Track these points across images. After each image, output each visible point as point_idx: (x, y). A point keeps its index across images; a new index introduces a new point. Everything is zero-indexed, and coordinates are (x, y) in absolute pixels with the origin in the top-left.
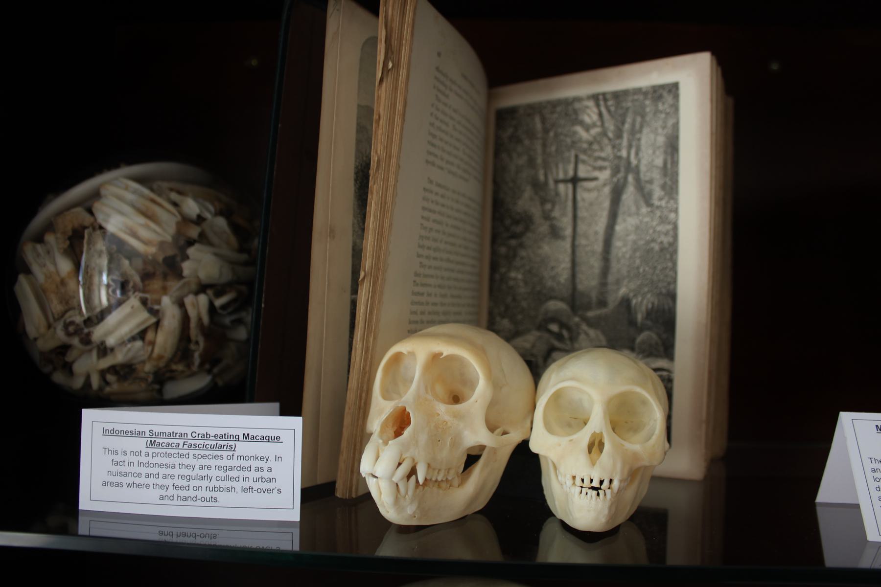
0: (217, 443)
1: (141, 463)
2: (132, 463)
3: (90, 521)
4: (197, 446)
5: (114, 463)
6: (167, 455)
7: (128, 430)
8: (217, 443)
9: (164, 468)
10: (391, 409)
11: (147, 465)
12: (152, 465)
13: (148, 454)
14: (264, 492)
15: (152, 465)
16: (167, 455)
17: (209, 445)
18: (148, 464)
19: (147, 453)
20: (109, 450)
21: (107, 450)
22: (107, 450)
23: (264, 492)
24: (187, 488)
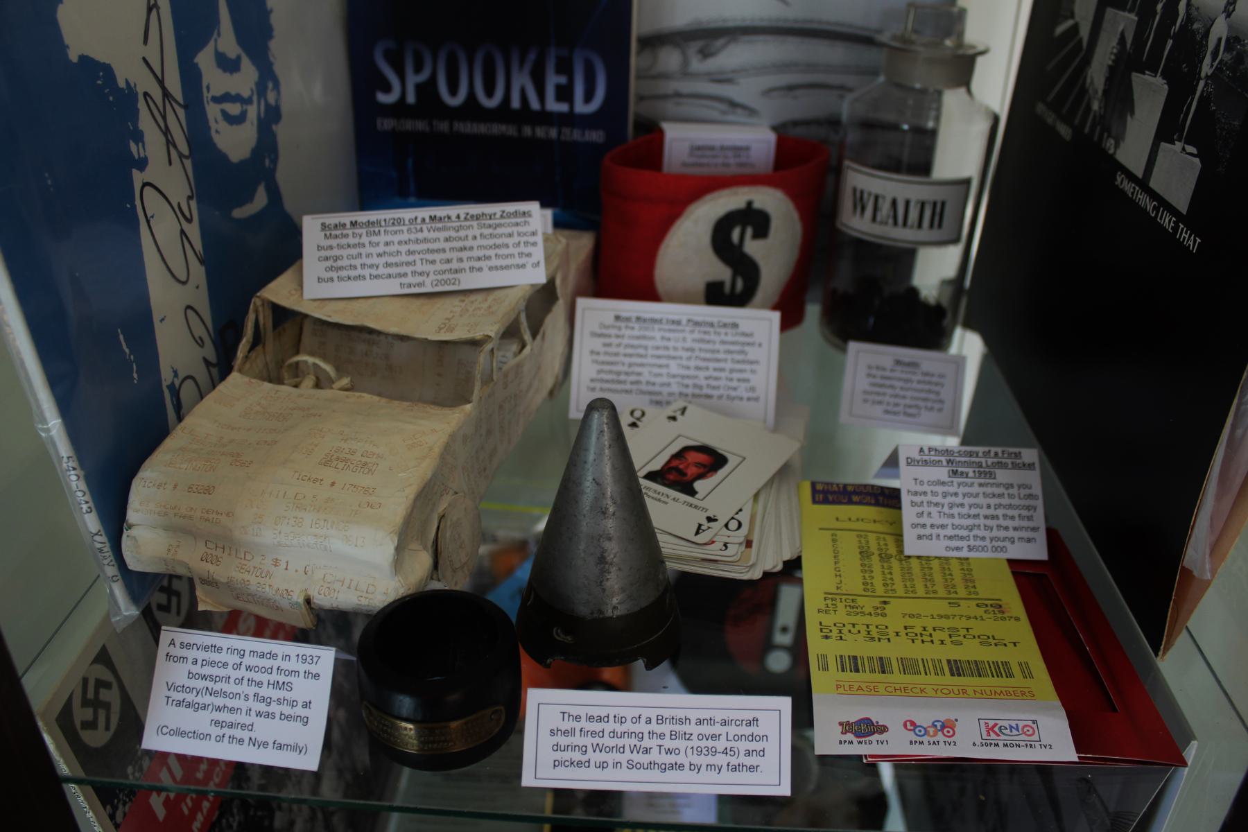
0: (319, 248)
1: (600, 767)
2: (619, 764)
3: (727, 740)
4: (227, 694)
5: (730, 768)
6: (677, 766)
7: (233, 691)
8: (756, 362)
9: (186, 738)
10: (1092, 79)
11: (750, 738)
12: (758, 738)
13: (650, 720)
14: (707, 740)
15: (758, 738)
16: (677, 766)
17: (309, 663)
18: (752, 736)
19: (648, 719)
20: (569, 716)
21: (566, 715)
22: (566, 715)
23: (707, 740)
24: (601, 734)
